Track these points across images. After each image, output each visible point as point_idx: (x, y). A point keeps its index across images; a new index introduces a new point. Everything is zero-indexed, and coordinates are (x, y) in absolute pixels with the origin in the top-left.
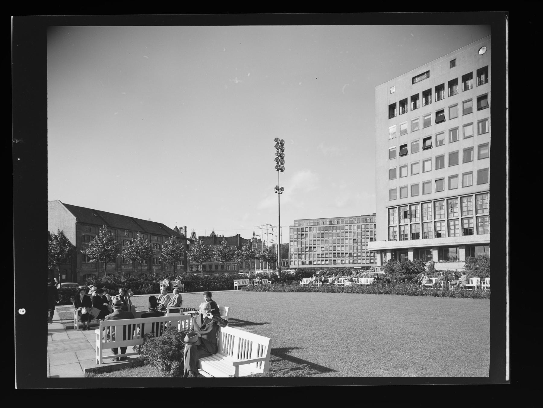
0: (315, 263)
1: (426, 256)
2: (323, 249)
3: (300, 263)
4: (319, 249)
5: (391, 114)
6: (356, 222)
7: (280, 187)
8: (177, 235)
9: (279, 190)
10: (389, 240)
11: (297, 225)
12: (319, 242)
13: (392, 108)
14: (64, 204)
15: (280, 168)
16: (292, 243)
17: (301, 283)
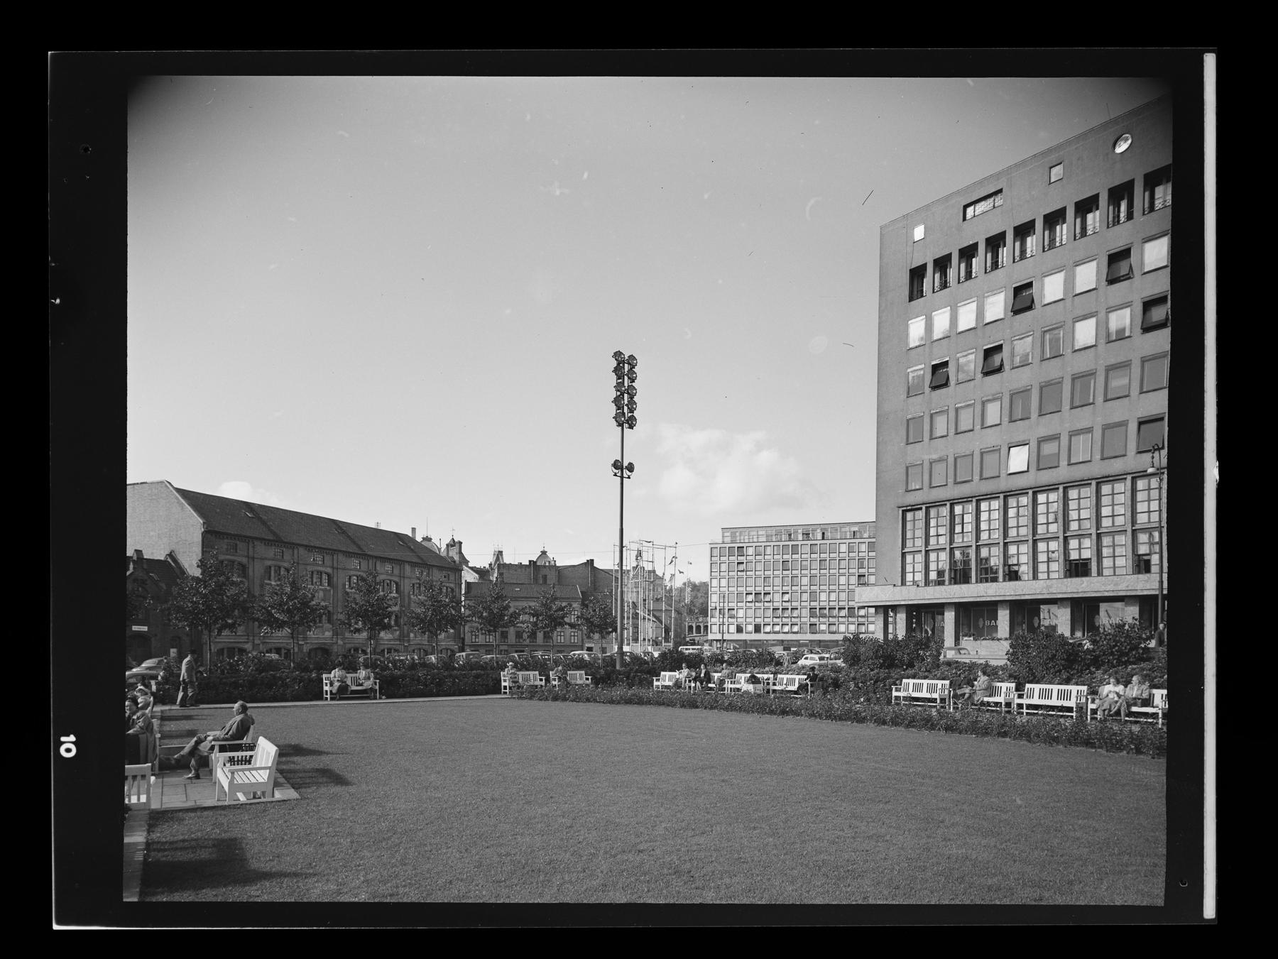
0: (768, 629)
1: (987, 623)
2: (786, 597)
3: (733, 629)
4: (777, 597)
5: (915, 292)
6: (866, 535)
7: (625, 464)
8: (438, 565)
9: (622, 468)
10: (927, 582)
11: (728, 540)
12: (778, 581)
13: (917, 274)
14: (178, 490)
15: (626, 419)
16: (715, 583)
17: (655, 683)
